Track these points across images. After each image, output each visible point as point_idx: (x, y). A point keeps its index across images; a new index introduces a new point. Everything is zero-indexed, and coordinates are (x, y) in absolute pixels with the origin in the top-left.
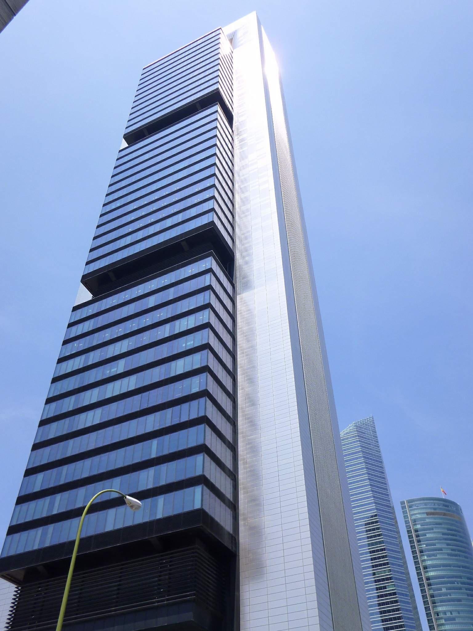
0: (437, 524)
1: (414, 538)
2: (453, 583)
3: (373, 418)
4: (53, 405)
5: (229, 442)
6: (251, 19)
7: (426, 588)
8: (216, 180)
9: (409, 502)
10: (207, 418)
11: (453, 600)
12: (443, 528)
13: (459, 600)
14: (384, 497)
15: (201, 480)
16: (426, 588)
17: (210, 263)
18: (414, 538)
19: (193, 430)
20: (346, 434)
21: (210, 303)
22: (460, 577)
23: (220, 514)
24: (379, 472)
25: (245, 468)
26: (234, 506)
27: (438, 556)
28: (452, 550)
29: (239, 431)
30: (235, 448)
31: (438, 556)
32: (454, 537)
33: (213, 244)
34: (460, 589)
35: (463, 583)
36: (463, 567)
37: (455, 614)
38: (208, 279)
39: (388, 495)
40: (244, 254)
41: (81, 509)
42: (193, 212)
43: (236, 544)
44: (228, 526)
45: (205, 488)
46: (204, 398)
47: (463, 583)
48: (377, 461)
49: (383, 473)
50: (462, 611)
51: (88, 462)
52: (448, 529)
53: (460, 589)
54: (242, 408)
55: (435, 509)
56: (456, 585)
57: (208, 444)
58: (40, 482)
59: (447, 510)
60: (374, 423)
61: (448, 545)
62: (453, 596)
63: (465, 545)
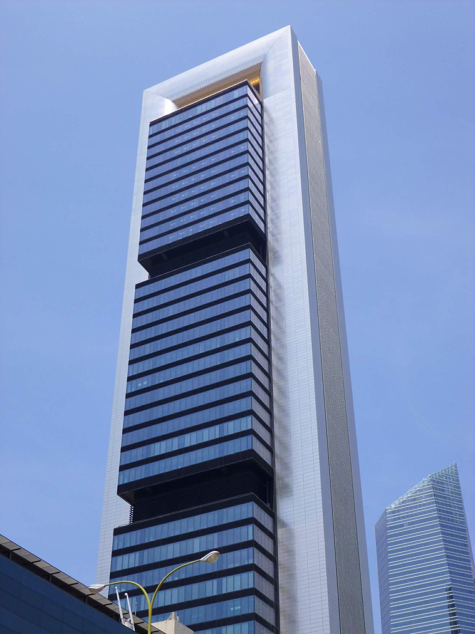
3: (456, 467)
5: (270, 532)
6: (285, 32)
8: (250, 170)
10: (255, 542)
14: (463, 556)
15: (251, 412)
17: (249, 254)
20: (403, 502)
21: (251, 391)
23: (264, 454)
24: (462, 545)
25: (283, 549)
26: (271, 449)
29: (280, 610)
30: (275, 559)
33: (249, 236)
38: (248, 269)
39: (465, 538)
40: (272, 138)
43: (273, 472)
44: (263, 230)
45: (255, 526)
46: (252, 503)
48: (459, 529)
49: (466, 545)
51: (202, 344)
54: (272, 232)
57: (253, 372)
58: (143, 335)
60: (457, 474)
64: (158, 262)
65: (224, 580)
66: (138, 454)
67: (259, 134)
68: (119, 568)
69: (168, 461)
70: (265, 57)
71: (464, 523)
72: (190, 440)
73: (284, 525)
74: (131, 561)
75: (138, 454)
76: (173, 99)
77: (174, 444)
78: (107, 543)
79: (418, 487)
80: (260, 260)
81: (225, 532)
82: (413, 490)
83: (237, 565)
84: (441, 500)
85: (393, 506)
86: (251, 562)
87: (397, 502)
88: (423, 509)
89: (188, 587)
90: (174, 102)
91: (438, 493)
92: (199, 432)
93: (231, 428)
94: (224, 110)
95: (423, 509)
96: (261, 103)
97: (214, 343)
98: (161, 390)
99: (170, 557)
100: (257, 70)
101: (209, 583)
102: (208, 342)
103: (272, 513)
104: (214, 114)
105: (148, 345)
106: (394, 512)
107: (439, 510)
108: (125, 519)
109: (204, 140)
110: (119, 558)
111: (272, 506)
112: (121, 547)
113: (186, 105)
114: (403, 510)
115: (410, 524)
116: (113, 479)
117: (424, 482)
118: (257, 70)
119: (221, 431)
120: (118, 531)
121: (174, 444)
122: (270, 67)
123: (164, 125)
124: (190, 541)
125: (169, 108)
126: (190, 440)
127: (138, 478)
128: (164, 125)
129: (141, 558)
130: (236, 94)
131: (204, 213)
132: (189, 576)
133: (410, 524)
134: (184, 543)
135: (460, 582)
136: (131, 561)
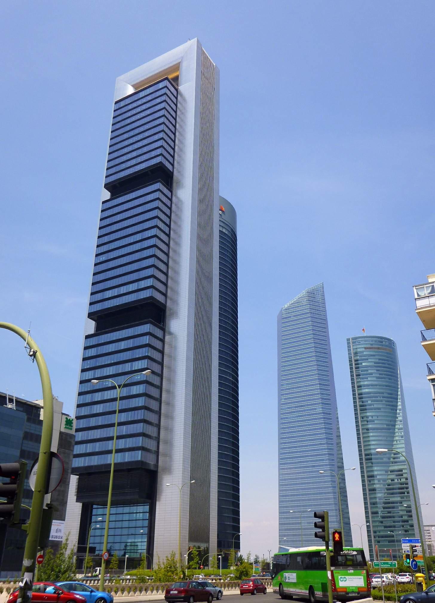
0: (372, 355)
1: (354, 366)
2: (377, 397)
4: (117, 104)
7: (357, 400)
9: (353, 339)
11: (375, 409)
12: (376, 358)
13: (379, 409)
16: (357, 400)
18: (354, 366)
19: (153, 230)
22: (383, 393)
27: (369, 379)
28: (380, 374)
31: (369, 379)
32: (391, 370)
34: (382, 401)
35: (383, 397)
36: (386, 386)
37: (374, 418)
41: (123, 387)
42: (123, 166)
47: (383, 397)
50: (380, 416)
52: (379, 359)
53: (382, 401)
55: (372, 345)
56: (379, 398)
58: (105, 231)
59: (380, 345)
61: (378, 370)
62: (375, 406)
63: (393, 371)
64: (117, 188)
65: (134, 363)
66: (99, 297)
67: (174, 110)
68: (87, 356)
69: (112, 301)
70: (182, 57)
71: (325, 315)
72: (123, 290)
73: (170, 334)
74: (92, 352)
75: (99, 297)
76: (133, 83)
77: (115, 292)
78: (81, 343)
79: (300, 295)
80: (167, 188)
81: (136, 339)
82: (297, 297)
83: (140, 356)
84: (311, 303)
85: (286, 306)
86: (147, 354)
87: (288, 304)
88: (304, 307)
89: (118, 366)
90: (133, 86)
91: (311, 299)
92: (128, 286)
93: (143, 284)
94: (153, 96)
95: (304, 307)
96: (177, 90)
97: (138, 237)
98: (111, 262)
99: (110, 351)
100: (177, 67)
101: (127, 364)
102: (135, 236)
103: (163, 329)
104: (149, 98)
105: (106, 237)
106: (286, 309)
107: (311, 309)
108: (92, 331)
109: (138, 116)
110: (87, 351)
111: (163, 325)
112: (88, 345)
113: (139, 88)
114: (292, 308)
115: (294, 316)
116: (85, 309)
117: (304, 293)
118: (177, 67)
119: (138, 286)
120: (87, 337)
121: (115, 292)
122: (184, 66)
123: (122, 104)
124: (120, 343)
125: (131, 90)
126: (123, 290)
127: (98, 309)
128: (122, 104)
129: (97, 351)
130: (161, 85)
131: (139, 160)
132: (118, 361)
133: (294, 316)
134: (117, 344)
135: (320, 348)
136: (92, 352)
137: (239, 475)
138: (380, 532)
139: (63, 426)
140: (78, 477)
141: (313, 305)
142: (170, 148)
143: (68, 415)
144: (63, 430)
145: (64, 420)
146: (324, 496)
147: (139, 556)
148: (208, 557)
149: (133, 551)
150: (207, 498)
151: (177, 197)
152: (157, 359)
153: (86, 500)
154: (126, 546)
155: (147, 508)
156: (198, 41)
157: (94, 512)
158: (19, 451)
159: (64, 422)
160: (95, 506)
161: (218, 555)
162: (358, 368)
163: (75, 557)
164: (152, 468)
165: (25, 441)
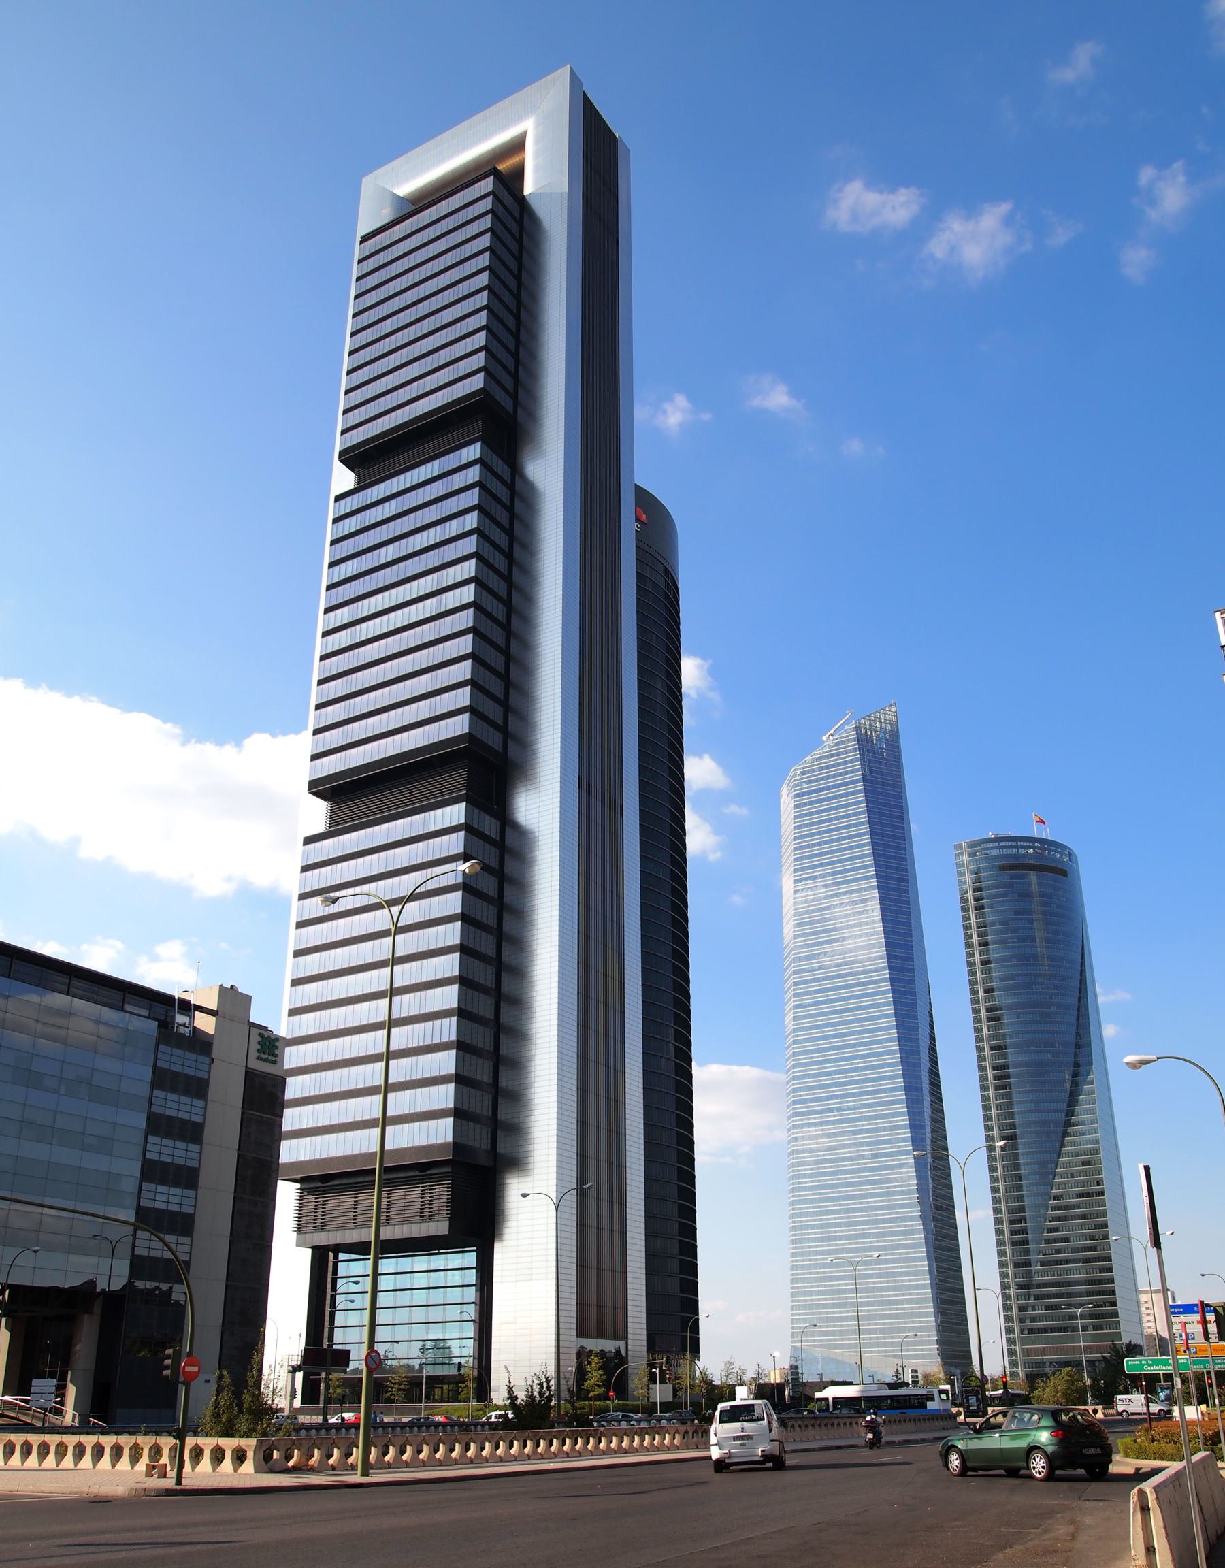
7: (979, 977)
108: (320, 826)
137: (694, 1177)
138: (1033, 1310)
139: (253, 1054)
140: (298, 1185)
141: (882, 824)
142: (507, 293)
143: (265, 1028)
144: (256, 1065)
145: (255, 1038)
146: (870, 1001)
147: (454, 1372)
148: (625, 1373)
149: (440, 1361)
150: (621, 1272)
151: (516, 826)
152: (484, 920)
153: (323, 1239)
154: (423, 1350)
155: (471, 1258)
156: (572, 72)
157: (342, 1269)
158: (145, 1116)
159: (255, 1047)
160: (342, 1256)
161: (652, 1366)
162: (983, 907)
163: (299, 1376)
164: (483, 1161)
165: (151, 1139)
